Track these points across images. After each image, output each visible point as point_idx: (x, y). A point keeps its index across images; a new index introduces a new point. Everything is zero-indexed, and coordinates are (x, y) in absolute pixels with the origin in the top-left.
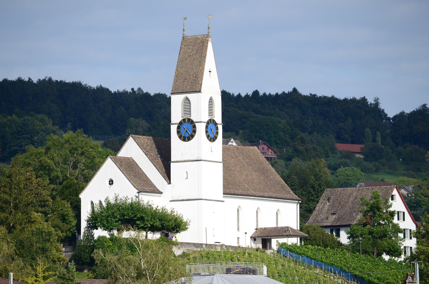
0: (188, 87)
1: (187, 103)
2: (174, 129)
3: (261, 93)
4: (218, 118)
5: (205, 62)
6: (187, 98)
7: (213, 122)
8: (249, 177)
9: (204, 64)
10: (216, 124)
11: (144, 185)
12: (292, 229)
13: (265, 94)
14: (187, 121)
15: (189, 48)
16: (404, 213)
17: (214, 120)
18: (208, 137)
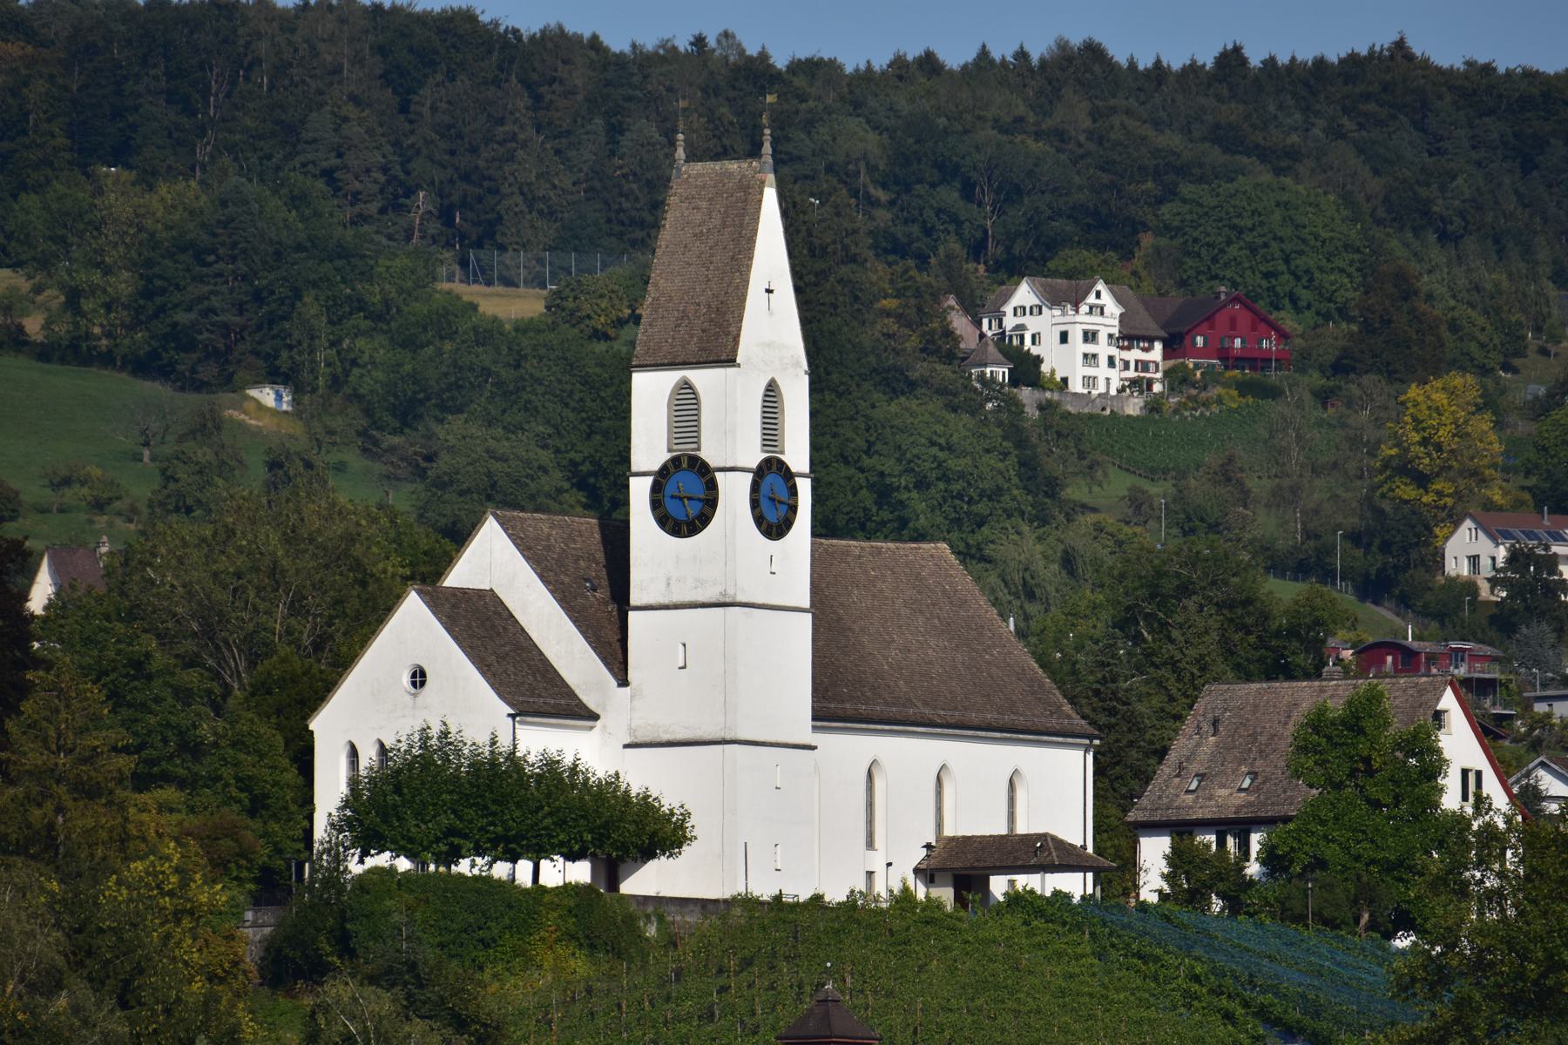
0: (693, 347)
1: (685, 403)
2: (640, 491)
3: (1255, 59)
4: (797, 455)
5: (751, 259)
6: (686, 385)
7: (780, 469)
8: (914, 656)
9: (749, 267)
10: (788, 476)
11: (537, 691)
12: (1060, 844)
13: (1270, 62)
14: (685, 465)
15: (698, 208)
16: (1479, 774)
17: (781, 463)
18: (759, 520)
